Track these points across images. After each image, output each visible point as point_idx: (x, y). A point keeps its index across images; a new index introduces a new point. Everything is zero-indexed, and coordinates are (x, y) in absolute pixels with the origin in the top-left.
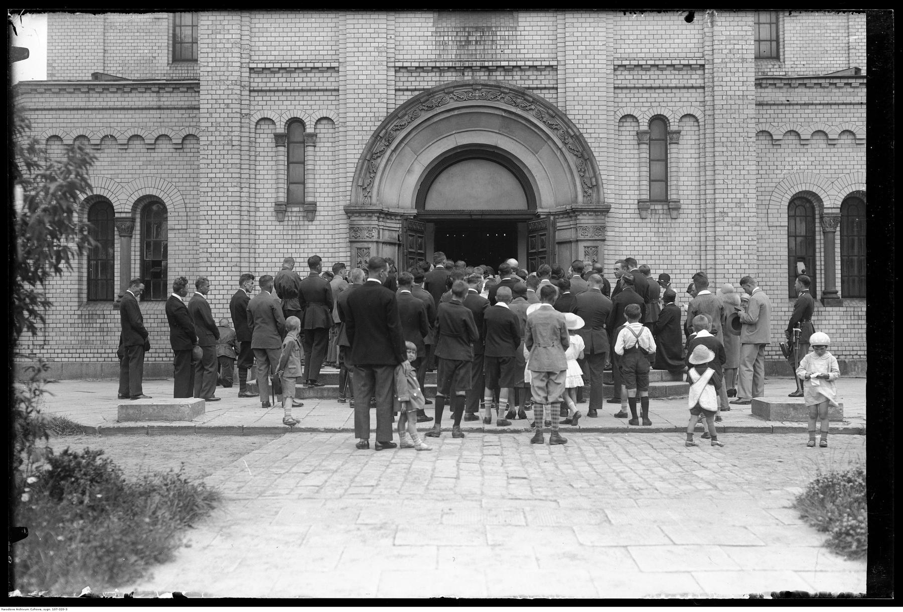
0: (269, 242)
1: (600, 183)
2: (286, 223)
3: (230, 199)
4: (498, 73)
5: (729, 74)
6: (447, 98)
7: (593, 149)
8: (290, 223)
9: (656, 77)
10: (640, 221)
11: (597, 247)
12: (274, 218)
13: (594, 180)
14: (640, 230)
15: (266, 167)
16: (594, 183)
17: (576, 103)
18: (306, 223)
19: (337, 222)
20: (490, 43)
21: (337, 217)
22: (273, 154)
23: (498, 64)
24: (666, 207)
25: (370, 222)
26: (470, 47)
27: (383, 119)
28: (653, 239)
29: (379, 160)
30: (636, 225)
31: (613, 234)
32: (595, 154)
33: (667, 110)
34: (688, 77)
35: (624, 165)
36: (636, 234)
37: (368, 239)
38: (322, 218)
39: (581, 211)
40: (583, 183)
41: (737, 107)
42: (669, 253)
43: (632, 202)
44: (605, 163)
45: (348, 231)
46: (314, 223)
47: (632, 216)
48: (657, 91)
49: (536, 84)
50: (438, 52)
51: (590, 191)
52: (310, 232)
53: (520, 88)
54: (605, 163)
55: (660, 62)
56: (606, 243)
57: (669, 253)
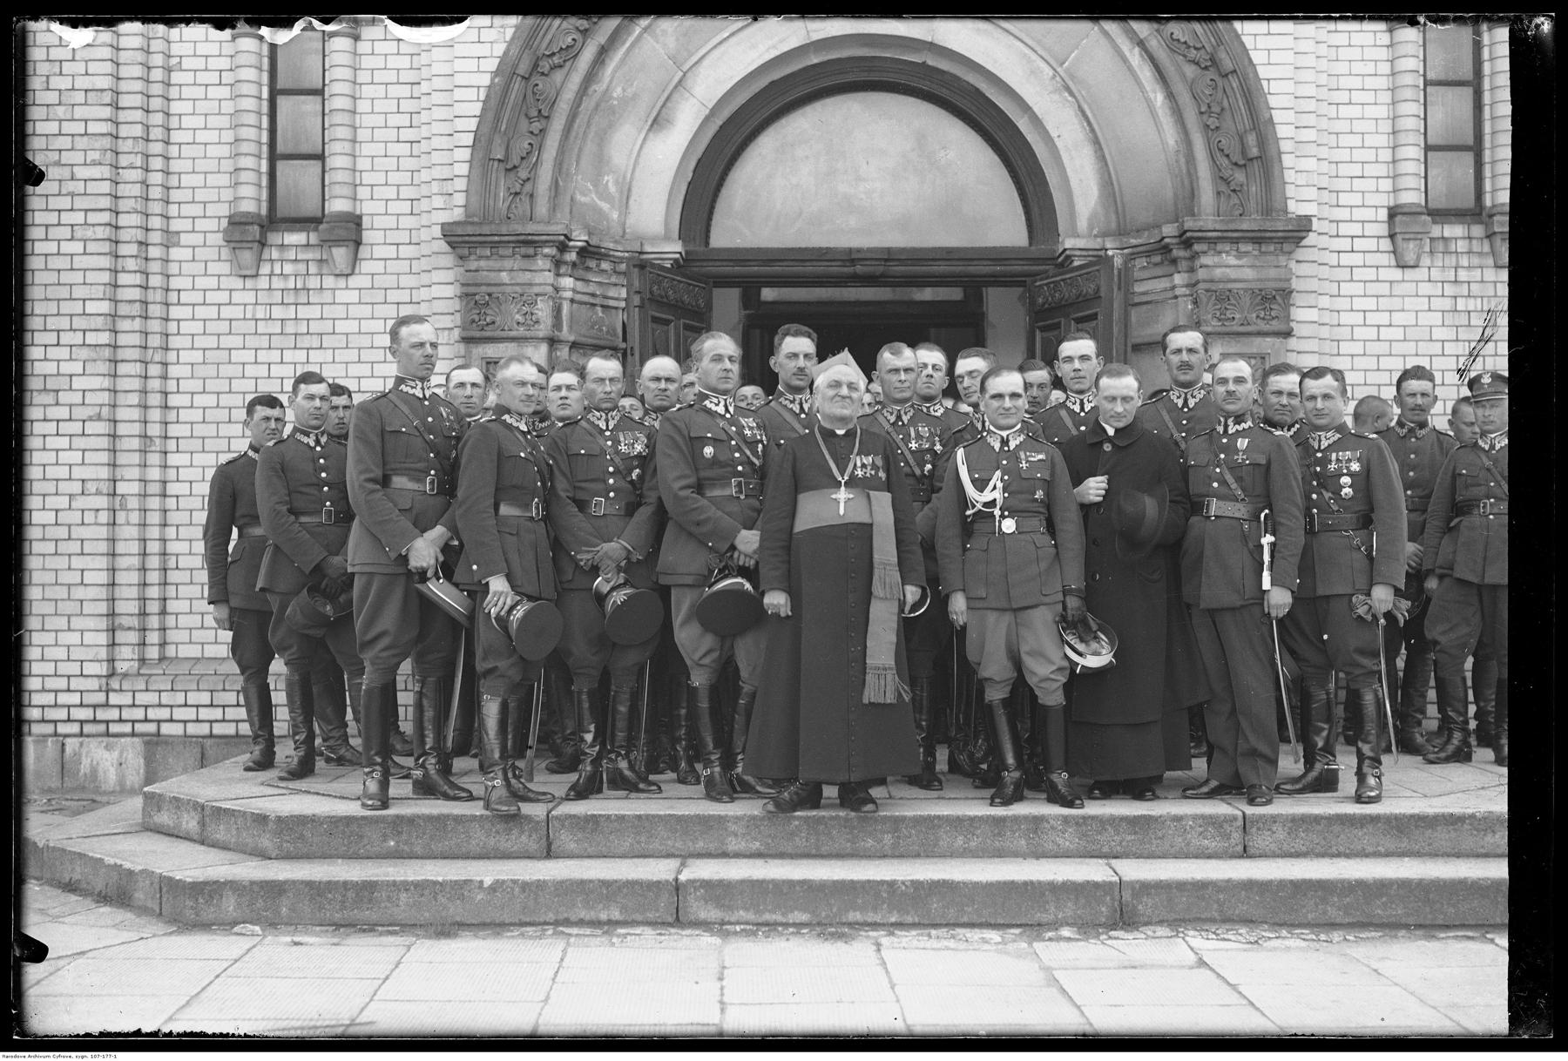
0: (211, 342)
1: (1272, 152)
2: (263, 283)
3: (80, 203)
8: (277, 283)
10: (1397, 274)
12: (225, 268)
13: (1251, 139)
14: (1396, 303)
15: (202, 107)
16: (1254, 152)
18: (329, 282)
19: (425, 279)
21: (424, 264)
22: (224, 63)
24: (1478, 230)
25: (526, 277)
28: (1439, 333)
29: (558, 76)
31: (1312, 315)
35: (1343, 97)
36: (1383, 318)
37: (521, 331)
38: (378, 267)
39: (1214, 241)
40: (1215, 151)
43: (1368, 214)
44: (1288, 86)
45: (457, 305)
46: (354, 281)
47: (1372, 259)
51: (1240, 176)
52: (339, 311)
54: (1288, 86)
56: (1293, 343)
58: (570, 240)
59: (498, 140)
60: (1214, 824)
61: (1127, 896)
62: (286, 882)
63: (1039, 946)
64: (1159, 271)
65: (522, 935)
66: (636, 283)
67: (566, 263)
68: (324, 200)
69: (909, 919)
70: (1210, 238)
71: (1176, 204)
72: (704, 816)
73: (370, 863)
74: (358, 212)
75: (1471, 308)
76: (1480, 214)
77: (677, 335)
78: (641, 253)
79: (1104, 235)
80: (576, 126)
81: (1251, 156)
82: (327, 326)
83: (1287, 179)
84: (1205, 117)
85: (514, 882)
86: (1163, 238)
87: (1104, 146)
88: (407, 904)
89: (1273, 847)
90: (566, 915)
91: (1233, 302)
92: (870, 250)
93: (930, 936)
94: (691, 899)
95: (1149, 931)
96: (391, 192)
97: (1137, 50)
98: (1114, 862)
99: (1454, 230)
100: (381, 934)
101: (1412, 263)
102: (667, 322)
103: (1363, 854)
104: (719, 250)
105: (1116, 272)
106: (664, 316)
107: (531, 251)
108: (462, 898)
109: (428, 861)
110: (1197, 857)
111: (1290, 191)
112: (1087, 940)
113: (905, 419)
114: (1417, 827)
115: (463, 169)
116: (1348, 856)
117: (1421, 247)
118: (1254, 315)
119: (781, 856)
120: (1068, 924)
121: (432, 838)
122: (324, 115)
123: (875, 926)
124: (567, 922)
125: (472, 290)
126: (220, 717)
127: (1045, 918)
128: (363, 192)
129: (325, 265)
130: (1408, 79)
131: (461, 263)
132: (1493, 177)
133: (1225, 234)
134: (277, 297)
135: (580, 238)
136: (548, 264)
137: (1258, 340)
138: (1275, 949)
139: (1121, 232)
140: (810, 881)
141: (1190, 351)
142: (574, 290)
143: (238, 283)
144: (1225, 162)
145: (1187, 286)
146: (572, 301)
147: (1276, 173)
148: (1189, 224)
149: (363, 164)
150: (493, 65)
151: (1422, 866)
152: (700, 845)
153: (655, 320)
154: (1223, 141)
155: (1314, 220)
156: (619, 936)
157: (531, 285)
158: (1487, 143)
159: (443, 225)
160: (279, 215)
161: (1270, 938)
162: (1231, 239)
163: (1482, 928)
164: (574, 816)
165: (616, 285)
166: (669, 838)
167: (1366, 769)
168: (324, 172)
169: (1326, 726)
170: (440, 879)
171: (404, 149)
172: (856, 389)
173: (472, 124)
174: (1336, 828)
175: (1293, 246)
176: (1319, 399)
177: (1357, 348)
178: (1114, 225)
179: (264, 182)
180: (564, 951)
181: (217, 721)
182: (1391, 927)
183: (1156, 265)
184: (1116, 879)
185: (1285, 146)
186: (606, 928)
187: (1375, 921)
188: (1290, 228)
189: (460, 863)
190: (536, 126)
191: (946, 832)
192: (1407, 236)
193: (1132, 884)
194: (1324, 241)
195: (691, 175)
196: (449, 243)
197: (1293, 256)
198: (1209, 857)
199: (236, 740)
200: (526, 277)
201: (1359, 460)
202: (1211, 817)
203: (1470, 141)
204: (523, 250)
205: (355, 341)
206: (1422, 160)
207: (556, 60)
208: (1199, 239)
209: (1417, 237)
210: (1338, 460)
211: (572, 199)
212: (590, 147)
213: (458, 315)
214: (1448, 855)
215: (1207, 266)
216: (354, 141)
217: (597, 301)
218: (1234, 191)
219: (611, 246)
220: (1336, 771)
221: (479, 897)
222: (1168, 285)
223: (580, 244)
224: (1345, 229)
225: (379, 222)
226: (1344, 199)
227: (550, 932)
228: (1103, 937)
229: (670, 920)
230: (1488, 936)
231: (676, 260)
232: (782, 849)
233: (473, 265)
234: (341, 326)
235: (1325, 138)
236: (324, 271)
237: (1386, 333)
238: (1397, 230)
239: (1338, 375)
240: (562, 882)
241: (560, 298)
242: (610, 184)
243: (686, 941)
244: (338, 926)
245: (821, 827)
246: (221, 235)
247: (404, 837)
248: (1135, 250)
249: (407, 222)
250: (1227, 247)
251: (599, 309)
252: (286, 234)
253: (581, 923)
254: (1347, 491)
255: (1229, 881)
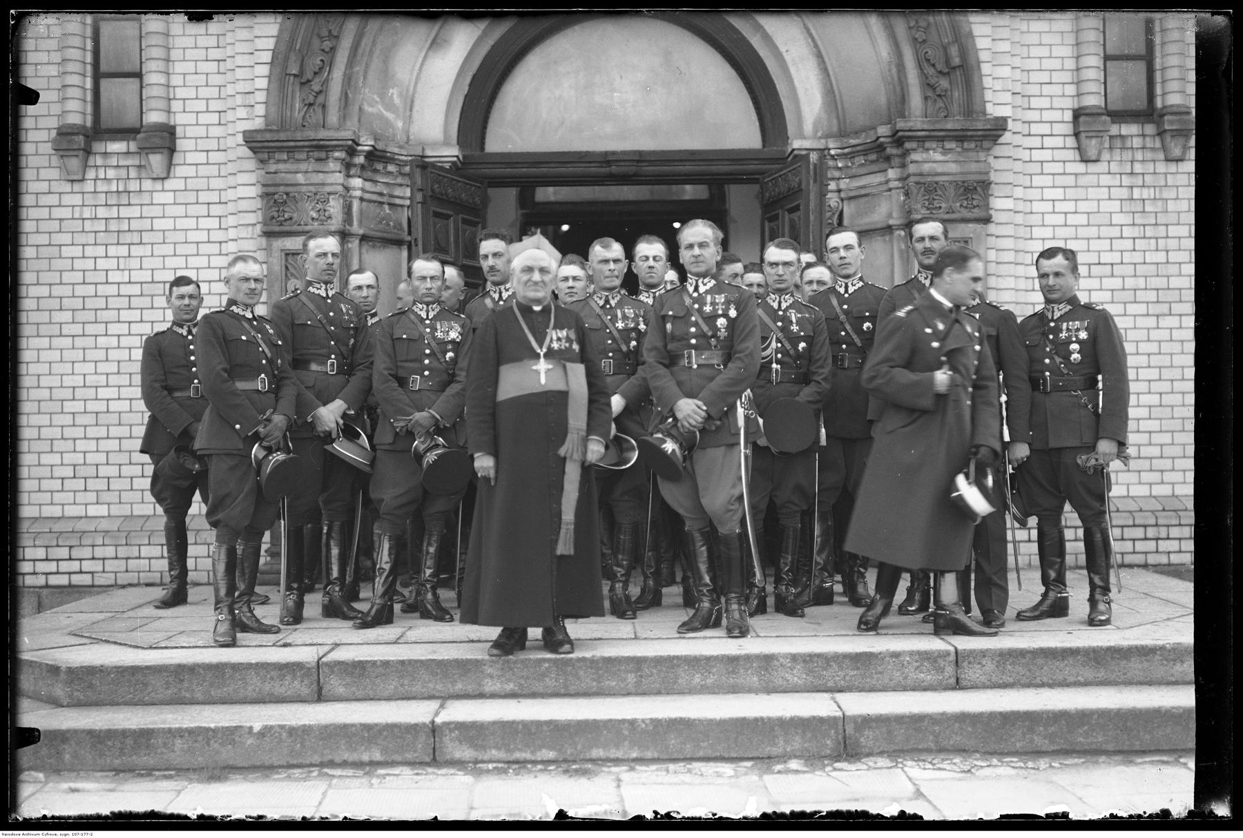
1: (973, 62)
2: (89, 186)
8: (102, 187)
10: (1081, 168)
12: (55, 173)
13: (954, 51)
14: (1080, 193)
18: (147, 185)
19: (232, 181)
21: (231, 168)
24: (1150, 129)
25: (319, 178)
28: (1117, 219)
36: (1069, 206)
38: (191, 171)
40: (923, 62)
43: (1056, 115)
45: (258, 203)
46: (169, 184)
51: (944, 83)
52: (156, 211)
56: (992, 228)
58: (358, 145)
59: (293, 57)
60: (928, 659)
61: (850, 729)
62: (68, 731)
63: (767, 778)
64: (875, 168)
65: (289, 777)
66: (419, 181)
67: (355, 165)
68: (142, 113)
69: (649, 755)
70: (919, 137)
71: (889, 109)
72: (462, 660)
73: (153, 709)
74: (172, 123)
75: (1145, 196)
76: (1152, 115)
77: (456, 230)
78: (423, 157)
79: (827, 136)
80: (363, 44)
81: (953, 64)
82: (146, 224)
83: (986, 85)
84: (914, 31)
85: (282, 727)
86: (878, 138)
87: (826, 60)
88: (182, 750)
89: (983, 679)
90: (330, 757)
91: (939, 192)
92: (624, 153)
93: (667, 771)
94: (446, 740)
95: (870, 761)
96: (201, 106)
98: (838, 696)
100: (157, 779)
101: (1094, 158)
102: (447, 217)
103: (1064, 684)
105: (812, 167)
106: (445, 212)
107: (323, 155)
108: (233, 742)
109: (207, 707)
110: (914, 689)
111: (988, 95)
112: (813, 771)
113: (613, 303)
114: (1112, 658)
115: (263, 83)
116: (1051, 686)
117: (1102, 143)
118: (958, 204)
119: (533, 695)
120: (796, 757)
121: (211, 685)
122: (141, 37)
123: (617, 761)
124: (332, 764)
125: (272, 190)
126: (54, 570)
127: (775, 751)
128: (177, 106)
129: (143, 170)
131: (262, 166)
132: (1163, 82)
133: (933, 134)
134: (101, 199)
135: (366, 143)
137: (962, 226)
138: (986, 778)
139: (842, 134)
140: (556, 721)
141: (932, 238)
142: (363, 190)
143: (67, 187)
144: (931, 71)
145: (899, 180)
146: (362, 199)
147: (976, 79)
148: (901, 124)
149: (176, 80)
151: (1119, 695)
152: (459, 686)
153: (436, 214)
154: (930, 53)
155: (1010, 121)
156: (378, 776)
157: (323, 184)
158: (1158, 54)
159: (244, 132)
160: (103, 126)
161: (982, 767)
162: (938, 137)
163: (1176, 752)
164: (343, 662)
165: (401, 185)
166: (430, 681)
167: (1098, 597)
168: (141, 87)
169: (1059, 560)
170: (212, 726)
171: (212, 67)
172: (548, 272)
173: (271, 44)
174: (1040, 661)
175: (992, 143)
176: (1051, 277)
178: (835, 129)
179: (89, 97)
180: (324, 794)
181: (51, 573)
182: (1092, 753)
183: (872, 162)
184: (839, 714)
185: (983, 56)
186: (368, 768)
187: (1077, 749)
188: (989, 127)
189: (236, 709)
190: (327, 45)
191: (685, 671)
192: (1090, 134)
193: (854, 719)
194: (1017, 139)
195: (467, 88)
196: (250, 148)
197: (991, 152)
198: (925, 689)
199: (70, 590)
200: (319, 178)
201: (1086, 329)
202: (926, 652)
203: (1143, 52)
204: (316, 154)
205: (171, 237)
206: (1102, 68)
208: (910, 138)
209: (1098, 134)
210: (1068, 330)
211: (360, 109)
212: (376, 63)
213: (260, 212)
214: (1141, 683)
215: (916, 162)
216: (168, 60)
217: (385, 199)
218: (939, 96)
219: (396, 150)
220: (1067, 597)
221: (249, 742)
222: (883, 179)
223: (367, 148)
224: (1035, 129)
225: (190, 132)
226: (1035, 103)
227: (315, 774)
228: (828, 769)
229: (428, 759)
230: (1182, 760)
231: (453, 163)
232: (535, 689)
233: (273, 168)
234: (158, 224)
235: (1018, 50)
236: (143, 175)
237: (1072, 219)
238: (1081, 129)
239: (1070, 255)
240: (327, 727)
241: (351, 197)
242: (395, 96)
243: (441, 780)
244: (118, 771)
245: (569, 669)
246: (50, 145)
247: (186, 685)
248: (854, 149)
249: (216, 131)
250: (934, 145)
251: (386, 207)
252: (108, 143)
253: (344, 764)
254: (1076, 357)
255: (943, 714)
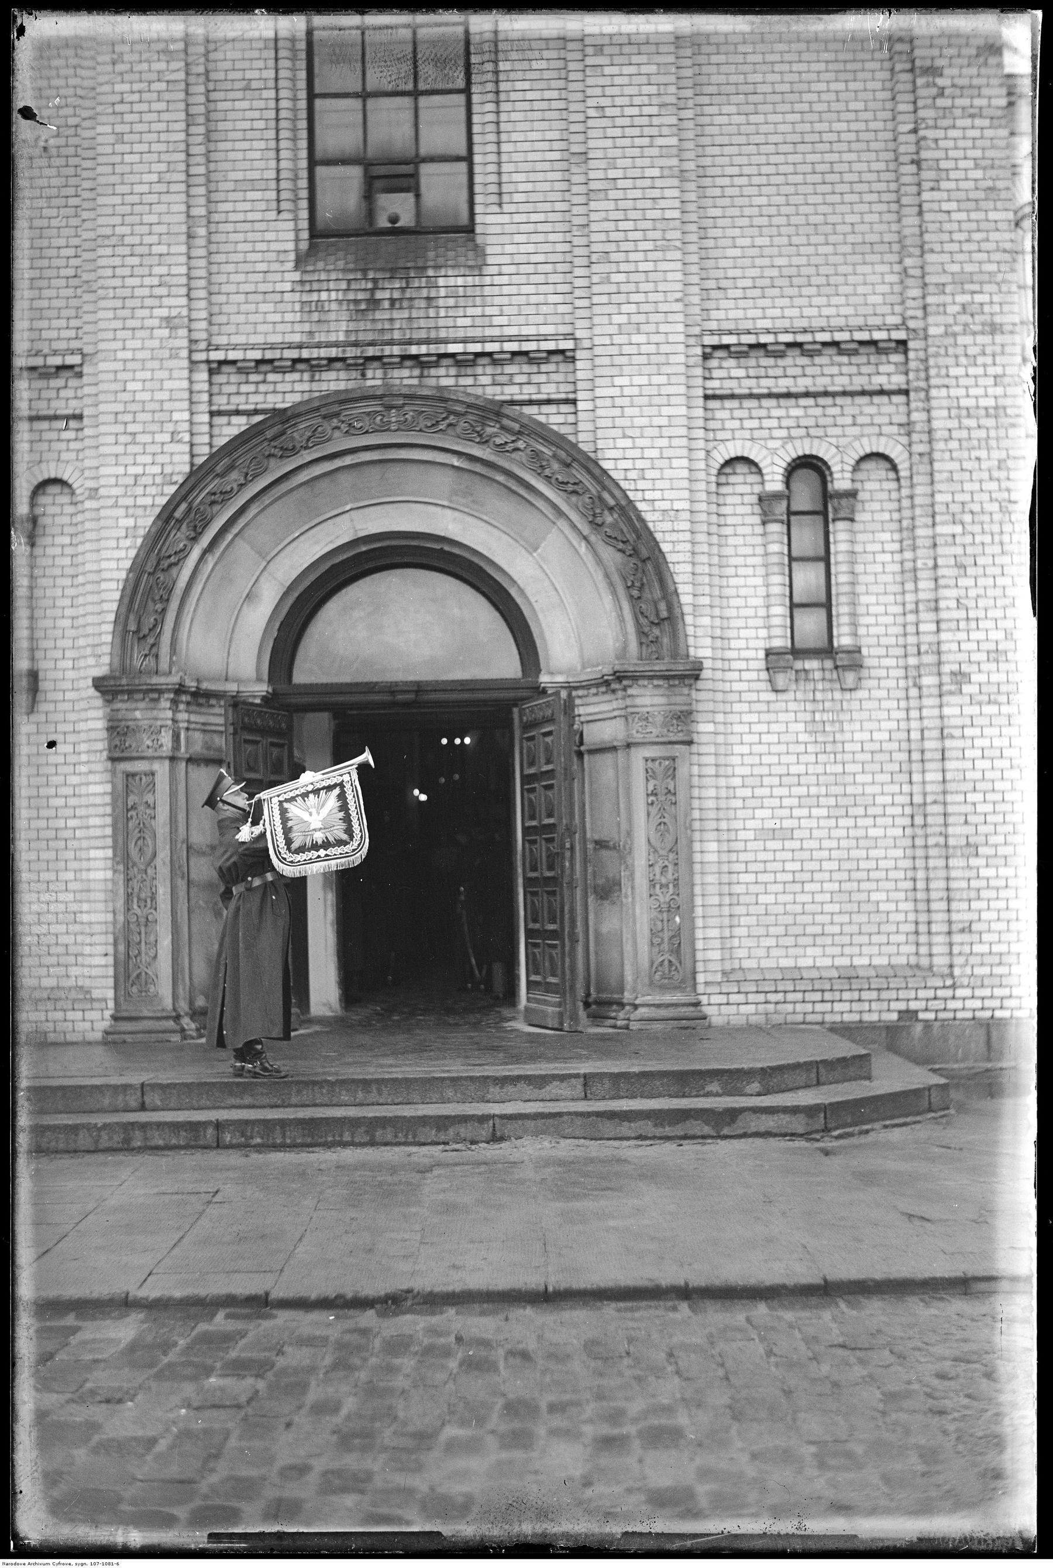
4: (442, 371)
5: (963, 360)
6: (327, 426)
7: (658, 536)
9: (798, 371)
10: (772, 696)
11: (674, 759)
13: (662, 606)
14: (772, 717)
16: (664, 614)
17: (617, 433)
20: (423, 304)
23: (442, 349)
24: (829, 664)
26: (378, 315)
27: (180, 479)
28: (803, 737)
29: (174, 571)
30: (763, 707)
32: (665, 547)
33: (825, 445)
34: (870, 369)
36: (764, 728)
37: (150, 753)
41: (983, 434)
42: (839, 768)
45: (104, 734)
47: (755, 686)
48: (803, 402)
49: (528, 392)
50: (307, 327)
51: (656, 631)
53: (492, 401)
55: (276, 354)
57: (839, 768)
92: (406, 683)
97: (583, 544)
99: (811, 664)
102: (256, 742)
104: (299, 686)
115: (109, 638)
130: (775, 559)
136: (168, 704)
150: (128, 564)
177: (745, 749)
207: (173, 559)
209: (786, 668)
237: (765, 738)
